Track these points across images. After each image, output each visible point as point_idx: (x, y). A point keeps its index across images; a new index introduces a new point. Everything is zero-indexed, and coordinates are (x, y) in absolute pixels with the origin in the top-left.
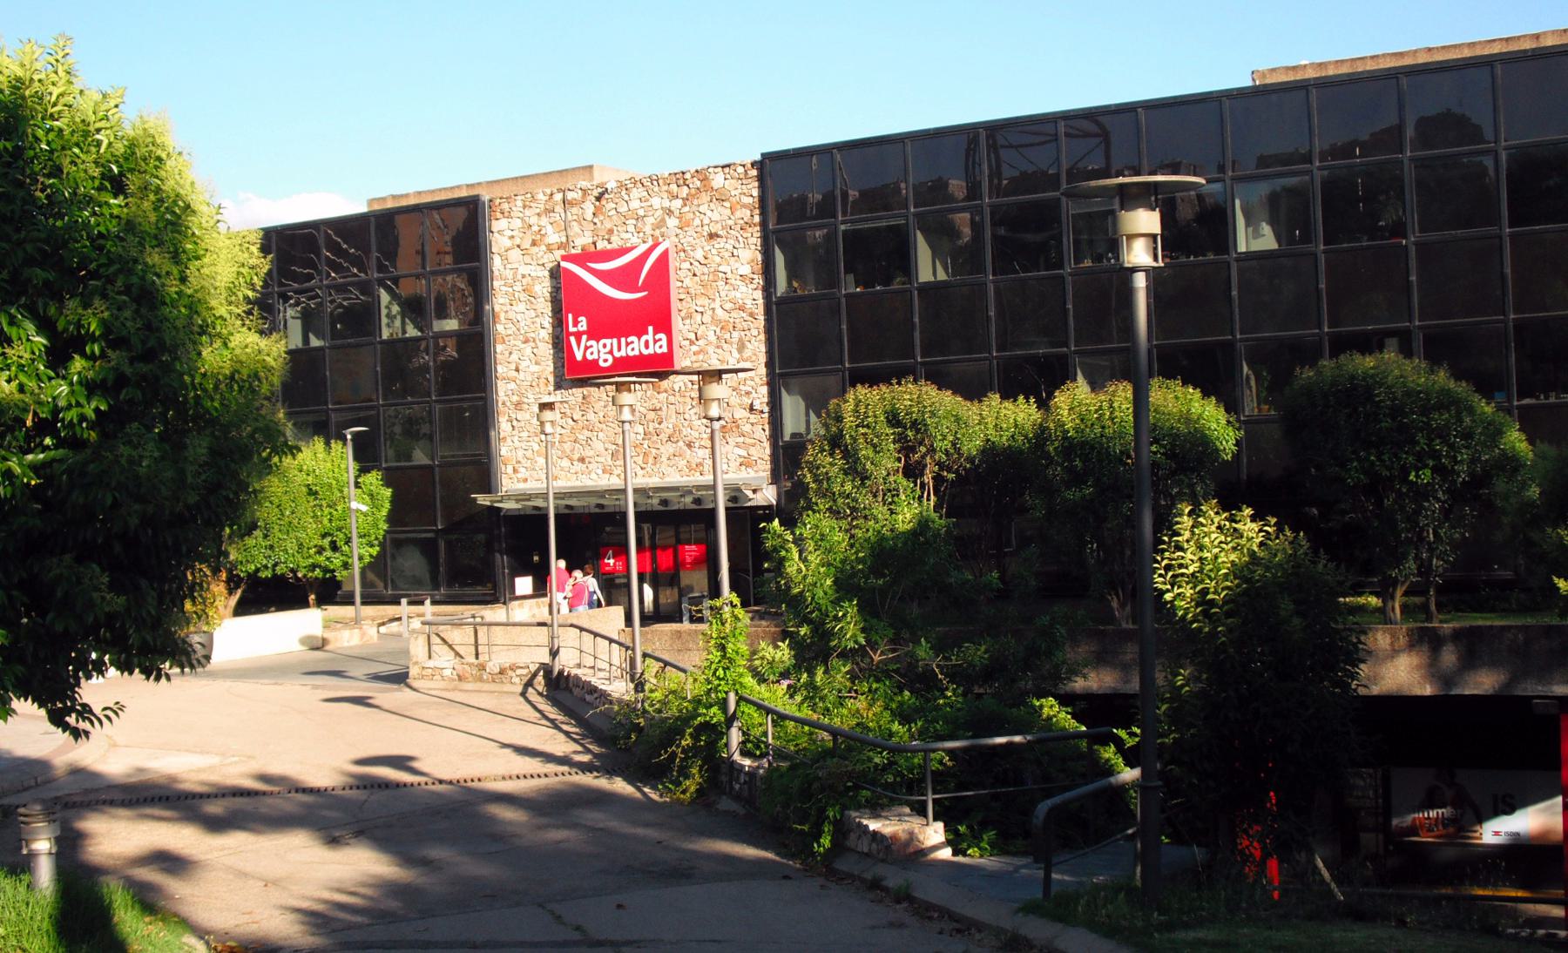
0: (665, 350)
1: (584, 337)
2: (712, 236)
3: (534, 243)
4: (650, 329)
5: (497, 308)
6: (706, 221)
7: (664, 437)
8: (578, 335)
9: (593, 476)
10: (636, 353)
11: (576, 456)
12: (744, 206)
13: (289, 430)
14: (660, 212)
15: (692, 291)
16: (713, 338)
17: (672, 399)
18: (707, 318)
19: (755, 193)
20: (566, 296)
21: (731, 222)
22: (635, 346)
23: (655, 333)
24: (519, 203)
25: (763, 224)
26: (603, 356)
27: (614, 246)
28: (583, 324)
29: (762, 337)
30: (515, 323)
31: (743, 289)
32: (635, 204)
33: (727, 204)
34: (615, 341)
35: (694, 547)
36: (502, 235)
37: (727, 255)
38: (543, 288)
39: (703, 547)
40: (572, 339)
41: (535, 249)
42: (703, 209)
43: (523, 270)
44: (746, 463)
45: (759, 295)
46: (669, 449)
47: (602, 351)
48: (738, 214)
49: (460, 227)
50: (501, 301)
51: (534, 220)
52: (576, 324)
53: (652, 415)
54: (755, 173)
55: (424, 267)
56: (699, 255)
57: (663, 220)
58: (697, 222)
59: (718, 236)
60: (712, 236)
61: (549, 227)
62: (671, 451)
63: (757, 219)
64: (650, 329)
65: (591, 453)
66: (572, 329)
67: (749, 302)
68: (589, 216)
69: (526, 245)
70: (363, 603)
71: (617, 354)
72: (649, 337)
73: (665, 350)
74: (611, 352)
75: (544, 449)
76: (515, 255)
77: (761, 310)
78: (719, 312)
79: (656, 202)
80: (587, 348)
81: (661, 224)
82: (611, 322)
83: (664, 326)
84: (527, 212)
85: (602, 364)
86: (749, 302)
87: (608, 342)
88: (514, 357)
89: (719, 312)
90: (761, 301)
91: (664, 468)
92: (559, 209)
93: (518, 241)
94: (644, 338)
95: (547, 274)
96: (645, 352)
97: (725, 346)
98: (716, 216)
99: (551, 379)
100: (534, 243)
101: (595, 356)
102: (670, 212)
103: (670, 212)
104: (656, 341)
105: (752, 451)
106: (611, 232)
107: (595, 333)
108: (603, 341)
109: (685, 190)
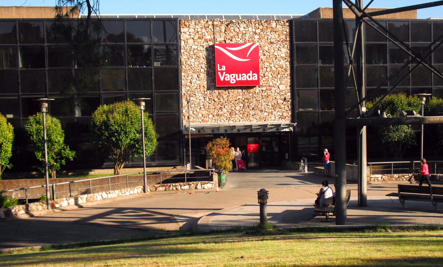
0: (256, 79)
1: (224, 73)
2: (271, 43)
3: (199, 38)
4: (251, 72)
5: (182, 60)
6: (269, 38)
7: (251, 108)
8: (222, 72)
9: (222, 121)
10: (245, 79)
11: (215, 114)
12: (283, 34)
13: (411, 91)
14: (251, 33)
15: (263, 60)
16: (270, 76)
17: (254, 95)
18: (268, 70)
19: (288, 31)
20: (212, 56)
21: (278, 39)
22: (245, 77)
23: (253, 73)
24: (193, 23)
25: (291, 41)
26: (232, 80)
27: (233, 42)
28: (224, 68)
29: (289, 77)
30: (190, 65)
31: (282, 61)
32: (242, 29)
33: (277, 33)
34: (237, 75)
35: (254, 145)
36: (186, 34)
37: (277, 49)
38: (203, 54)
39: (257, 145)
40: (219, 73)
41: (200, 40)
42: (268, 34)
43: (194, 47)
44: (282, 117)
45: (288, 63)
46: (252, 112)
47: (232, 78)
48: (281, 37)
49: (169, 27)
50: (184, 57)
51: (199, 30)
52: (221, 68)
53: (246, 101)
54: (288, 24)
55: (165, 41)
56: (266, 48)
57: (253, 36)
58: (266, 38)
59: (273, 43)
60: (271, 43)
61: (206, 33)
62: (254, 113)
63: (288, 39)
64: (251, 72)
65: (222, 113)
66: (219, 69)
67: (284, 66)
68: (223, 31)
69: (196, 38)
70: (147, 167)
71: (237, 79)
72: (251, 74)
73: (256, 79)
74: (235, 78)
75: (199, 110)
76: (191, 41)
77: (289, 68)
78: (273, 68)
79: (250, 29)
80: (225, 77)
81: (252, 37)
82: (234, 68)
83: (256, 70)
84: (197, 27)
85: (231, 82)
86: (284, 66)
87: (234, 75)
88: (190, 78)
89: (273, 68)
90: (289, 66)
91: (251, 118)
92: (211, 27)
93: (192, 37)
94: (248, 75)
95: (204, 49)
96: (249, 79)
97: (275, 79)
98: (273, 37)
99: (206, 86)
100: (199, 38)
101: (229, 79)
102: (255, 33)
103: (255, 33)
104: (253, 76)
105: (284, 114)
106: (232, 37)
107: (229, 71)
108: (232, 75)
109: (261, 27)
